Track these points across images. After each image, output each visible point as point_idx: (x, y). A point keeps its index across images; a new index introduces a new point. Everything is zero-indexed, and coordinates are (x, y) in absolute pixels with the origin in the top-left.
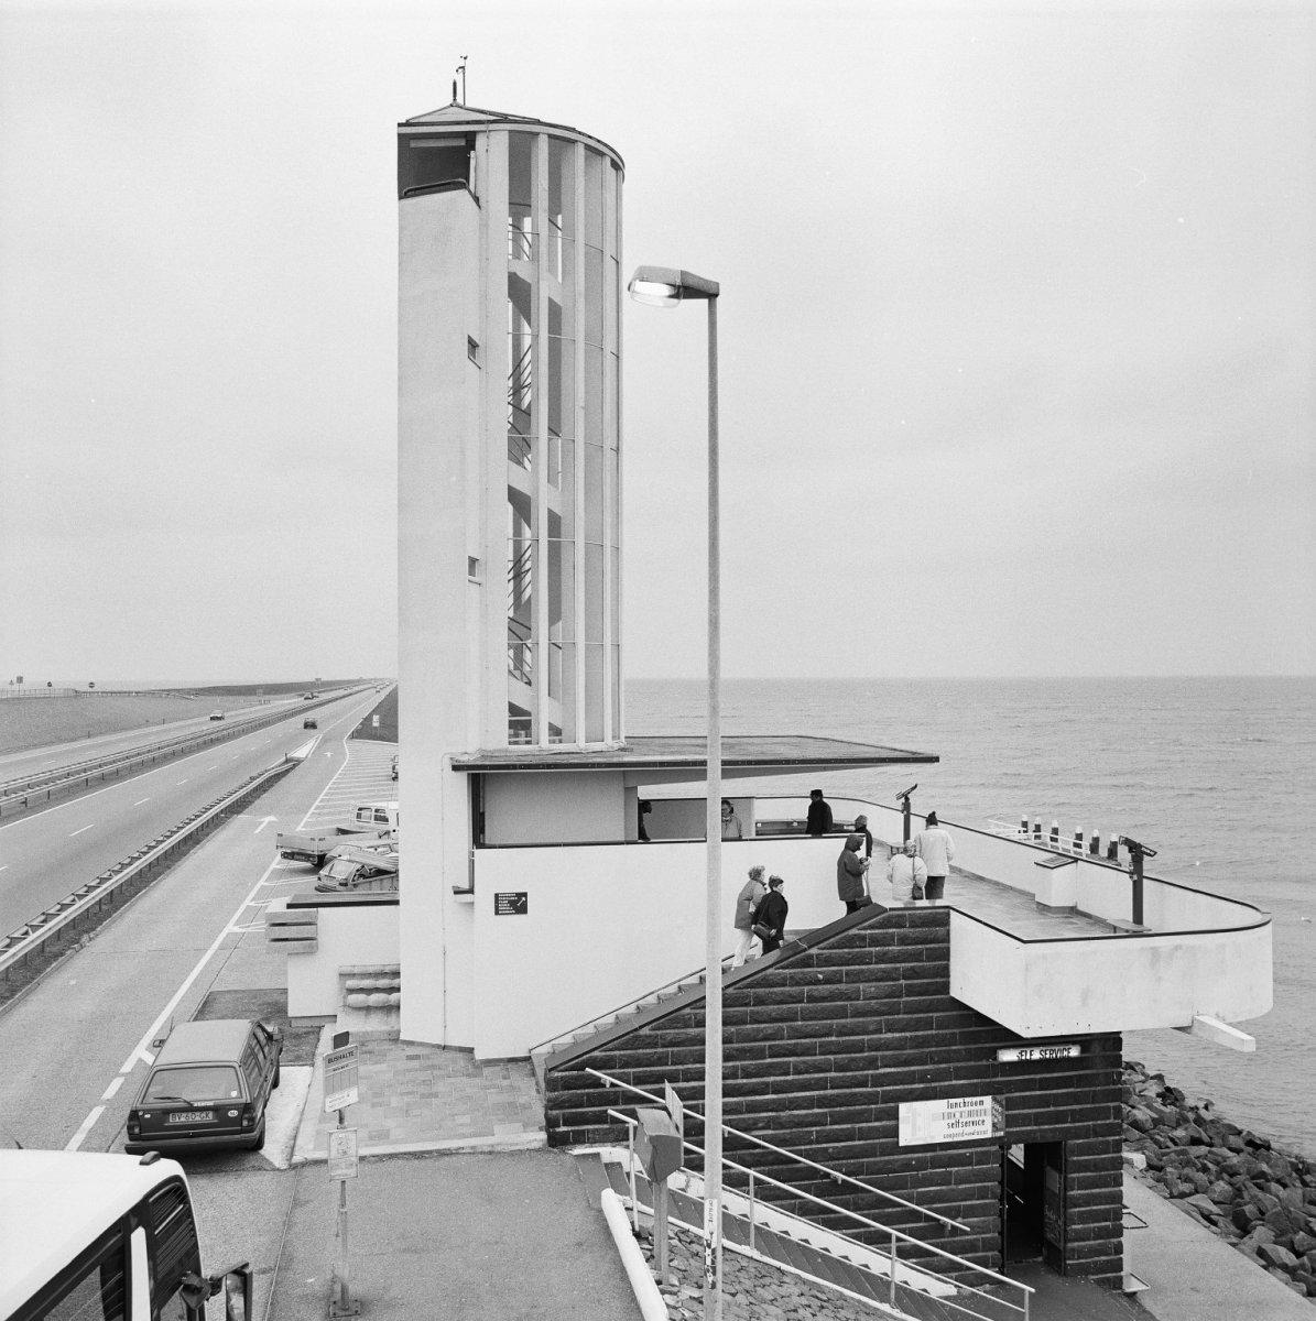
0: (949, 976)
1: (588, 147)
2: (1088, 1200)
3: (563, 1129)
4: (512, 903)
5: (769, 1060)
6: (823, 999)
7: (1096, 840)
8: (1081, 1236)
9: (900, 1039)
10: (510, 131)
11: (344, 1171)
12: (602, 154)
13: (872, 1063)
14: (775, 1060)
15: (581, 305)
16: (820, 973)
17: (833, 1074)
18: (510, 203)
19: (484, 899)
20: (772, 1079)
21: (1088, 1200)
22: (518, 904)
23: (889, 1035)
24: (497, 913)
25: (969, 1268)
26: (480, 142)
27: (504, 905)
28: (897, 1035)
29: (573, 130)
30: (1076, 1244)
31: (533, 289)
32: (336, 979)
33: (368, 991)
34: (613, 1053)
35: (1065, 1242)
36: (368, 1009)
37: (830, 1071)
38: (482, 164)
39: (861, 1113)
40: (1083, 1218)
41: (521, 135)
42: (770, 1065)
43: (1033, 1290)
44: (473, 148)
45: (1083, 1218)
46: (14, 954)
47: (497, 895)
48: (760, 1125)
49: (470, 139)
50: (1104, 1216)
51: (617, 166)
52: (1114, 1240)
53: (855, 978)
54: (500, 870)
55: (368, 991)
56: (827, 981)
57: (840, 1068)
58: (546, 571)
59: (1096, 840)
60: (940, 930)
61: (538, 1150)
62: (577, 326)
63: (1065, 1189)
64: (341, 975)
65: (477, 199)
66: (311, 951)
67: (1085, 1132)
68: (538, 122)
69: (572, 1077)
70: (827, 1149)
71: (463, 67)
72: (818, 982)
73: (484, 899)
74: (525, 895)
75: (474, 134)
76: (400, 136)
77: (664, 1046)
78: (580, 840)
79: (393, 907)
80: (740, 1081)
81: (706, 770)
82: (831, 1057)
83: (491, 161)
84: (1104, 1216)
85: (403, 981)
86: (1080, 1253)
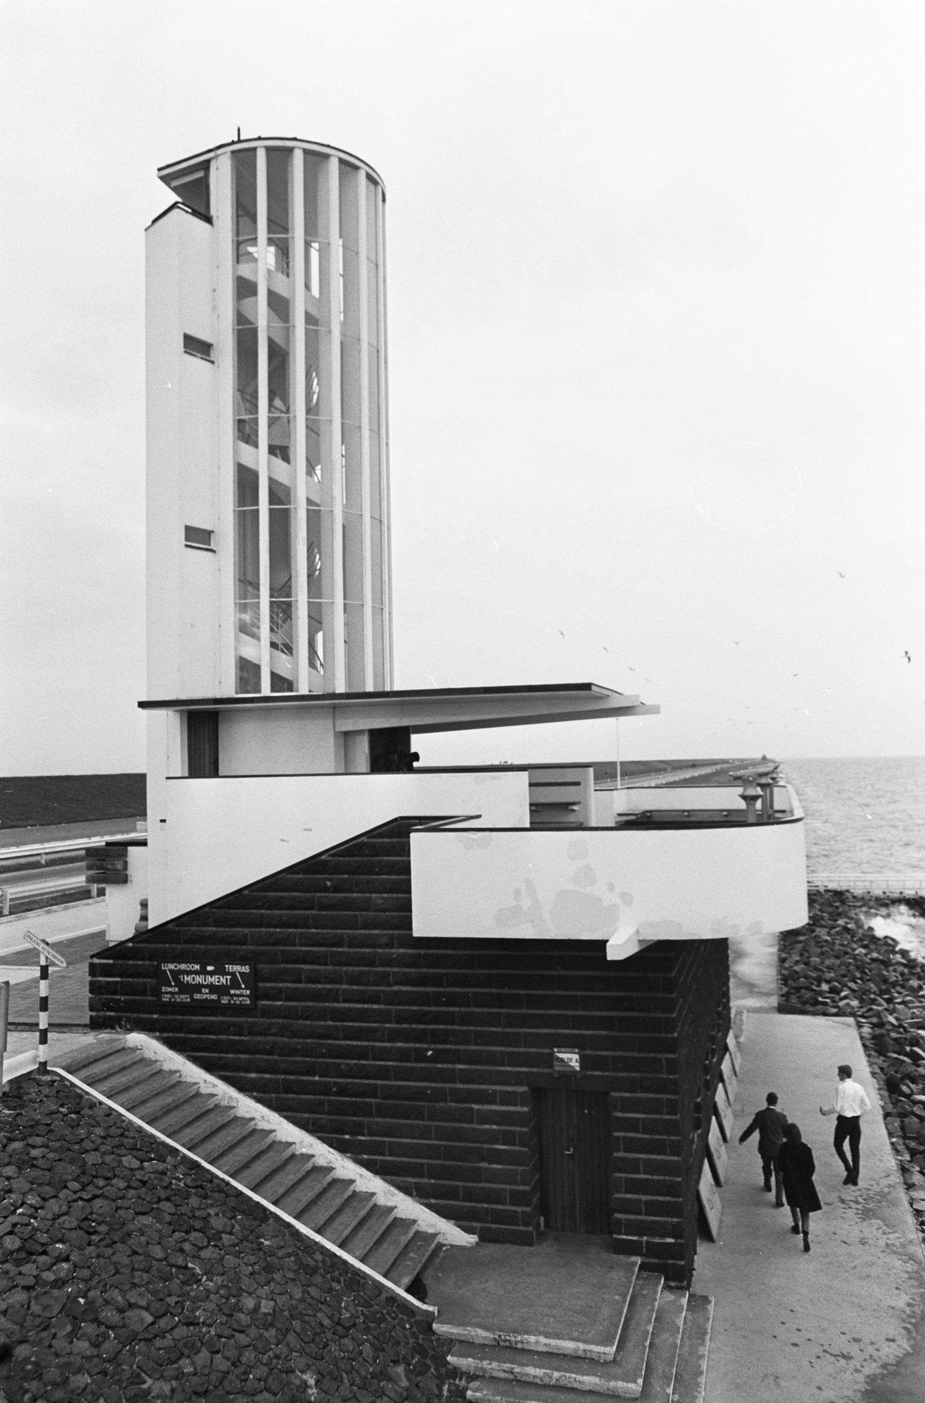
1: (341, 161)
6: (331, 907)
8: (628, 1207)
9: (412, 955)
10: (233, 152)
12: (357, 168)
13: (383, 979)
16: (329, 880)
17: (344, 987)
21: (634, 1166)
31: (291, 301)
34: (143, 945)
37: (341, 983)
39: (374, 1030)
42: (284, 971)
46: (58, 886)
48: (274, 1031)
53: (368, 887)
56: (336, 889)
57: (353, 980)
58: (277, 542)
61: (85, 1026)
67: (632, 1086)
70: (340, 1064)
72: (326, 889)
75: (208, 162)
77: (186, 943)
78: (256, 773)
81: (621, 763)
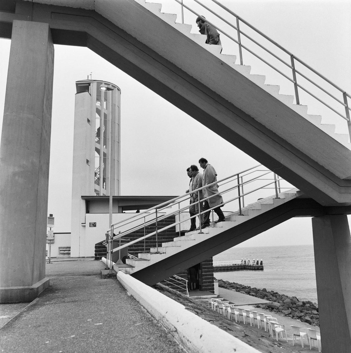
0: (175, 229)
2: (206, 275)
3: (98, 256)
4: (93, 225)
5: (139, 244)
7: (258, 261)
11: (51, 238)
12: (115, 87)
14: (140, 244)
15: (111, 114)
18: (32, 21)
19: (87, 225)
20: (140, 248)
21: (206, 275)
22: (94, 225)
23: (164, 240)
24: (90, 227)
25: (182, 288)
26: (91, 84)
27: (91, 225)
28: (165, 240)
29: (110, 83)
30: (204, 284)
32: (58, 249)
33: (65, 251)
35: (202, 284)
36: (64, 254)
38: (92, 89)
40: (206, 279)
41: (100, 83)
42: (140, 245)
43: (188, 281)
44: (90, 85)
45: (206, 279)
47: (90, 223)
49: (89, 84)
50: (210, 278)
51: (119, 90)
52: (212, 284)
54: (91, 217)
55: (65, 251)
59: (258, 261)
60: (173, 220)
62: (110, 118)
63: (202, 273)
64: (59, 248)
65: (90, 95)
66: (54, 244)
68: (102, 81)
69: (100, 246)
71: (91, 74)
73: (87, 225)
74: (96, 223)
75: (90, 83)
76: (76, 84)
79: (70, 234)
80: (133, 248)
82: (152, 244)
83: (93, 88)
84: (210, 278)
85: (71, 249)
86: (205, 286)
